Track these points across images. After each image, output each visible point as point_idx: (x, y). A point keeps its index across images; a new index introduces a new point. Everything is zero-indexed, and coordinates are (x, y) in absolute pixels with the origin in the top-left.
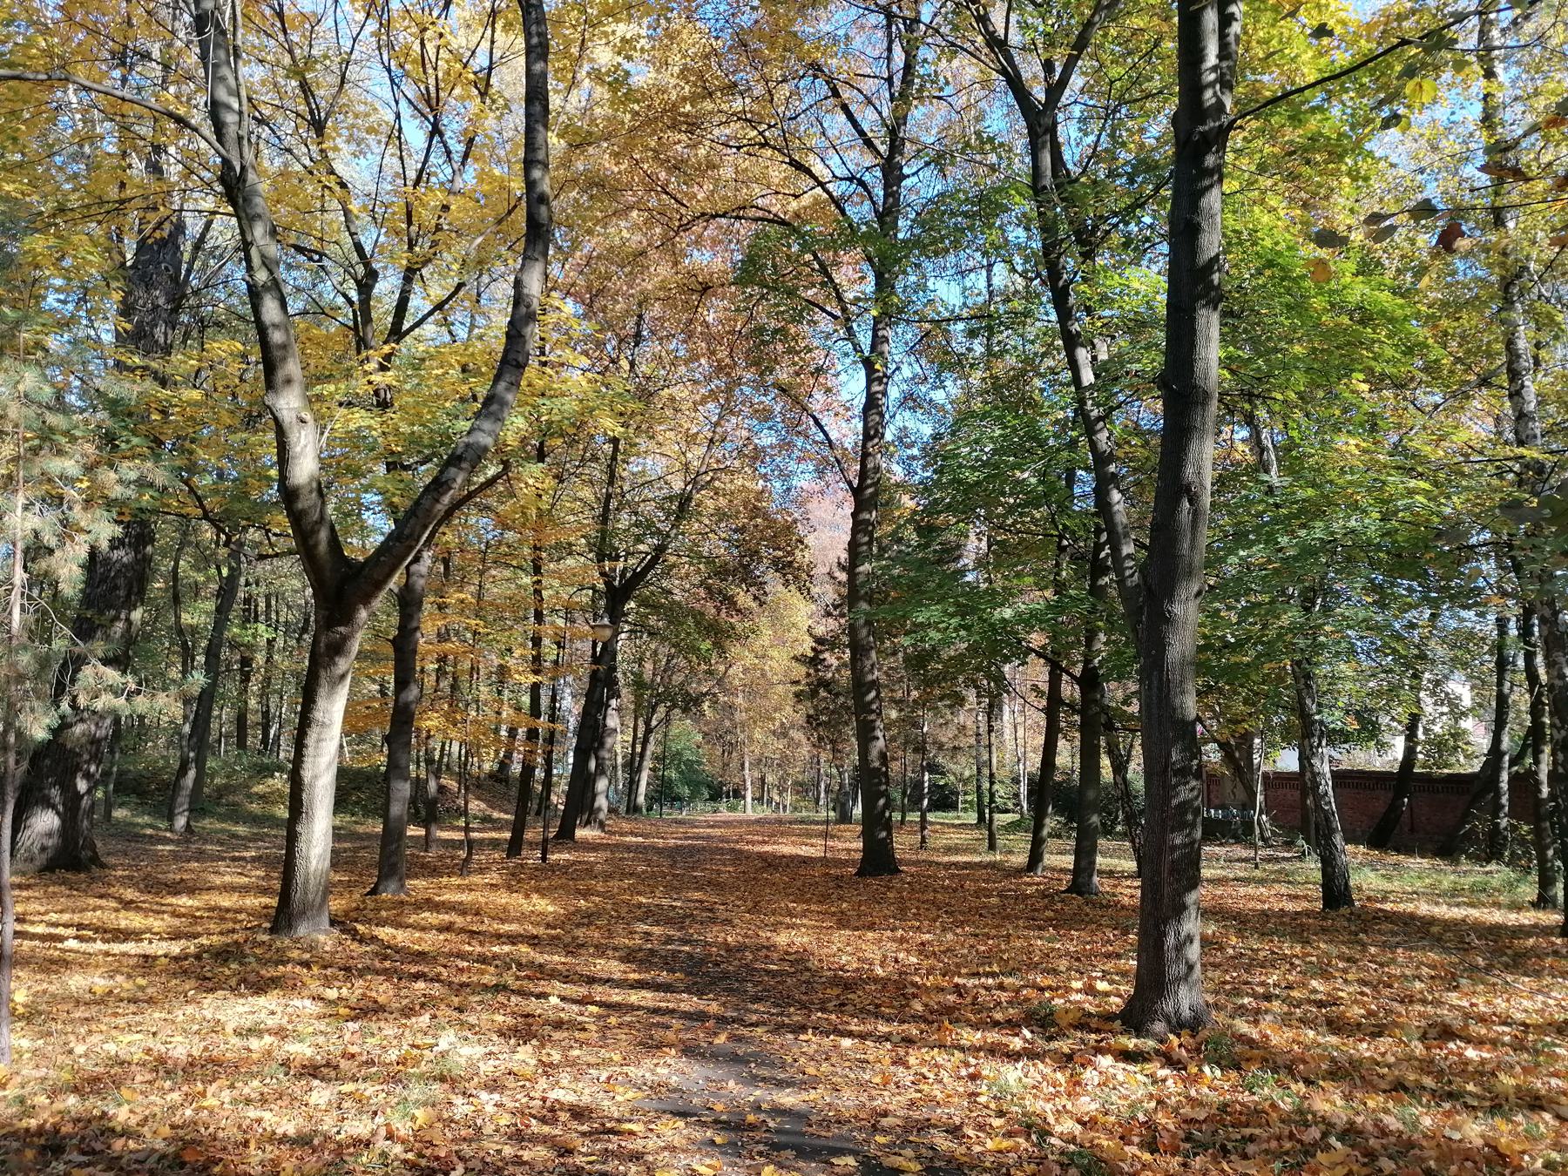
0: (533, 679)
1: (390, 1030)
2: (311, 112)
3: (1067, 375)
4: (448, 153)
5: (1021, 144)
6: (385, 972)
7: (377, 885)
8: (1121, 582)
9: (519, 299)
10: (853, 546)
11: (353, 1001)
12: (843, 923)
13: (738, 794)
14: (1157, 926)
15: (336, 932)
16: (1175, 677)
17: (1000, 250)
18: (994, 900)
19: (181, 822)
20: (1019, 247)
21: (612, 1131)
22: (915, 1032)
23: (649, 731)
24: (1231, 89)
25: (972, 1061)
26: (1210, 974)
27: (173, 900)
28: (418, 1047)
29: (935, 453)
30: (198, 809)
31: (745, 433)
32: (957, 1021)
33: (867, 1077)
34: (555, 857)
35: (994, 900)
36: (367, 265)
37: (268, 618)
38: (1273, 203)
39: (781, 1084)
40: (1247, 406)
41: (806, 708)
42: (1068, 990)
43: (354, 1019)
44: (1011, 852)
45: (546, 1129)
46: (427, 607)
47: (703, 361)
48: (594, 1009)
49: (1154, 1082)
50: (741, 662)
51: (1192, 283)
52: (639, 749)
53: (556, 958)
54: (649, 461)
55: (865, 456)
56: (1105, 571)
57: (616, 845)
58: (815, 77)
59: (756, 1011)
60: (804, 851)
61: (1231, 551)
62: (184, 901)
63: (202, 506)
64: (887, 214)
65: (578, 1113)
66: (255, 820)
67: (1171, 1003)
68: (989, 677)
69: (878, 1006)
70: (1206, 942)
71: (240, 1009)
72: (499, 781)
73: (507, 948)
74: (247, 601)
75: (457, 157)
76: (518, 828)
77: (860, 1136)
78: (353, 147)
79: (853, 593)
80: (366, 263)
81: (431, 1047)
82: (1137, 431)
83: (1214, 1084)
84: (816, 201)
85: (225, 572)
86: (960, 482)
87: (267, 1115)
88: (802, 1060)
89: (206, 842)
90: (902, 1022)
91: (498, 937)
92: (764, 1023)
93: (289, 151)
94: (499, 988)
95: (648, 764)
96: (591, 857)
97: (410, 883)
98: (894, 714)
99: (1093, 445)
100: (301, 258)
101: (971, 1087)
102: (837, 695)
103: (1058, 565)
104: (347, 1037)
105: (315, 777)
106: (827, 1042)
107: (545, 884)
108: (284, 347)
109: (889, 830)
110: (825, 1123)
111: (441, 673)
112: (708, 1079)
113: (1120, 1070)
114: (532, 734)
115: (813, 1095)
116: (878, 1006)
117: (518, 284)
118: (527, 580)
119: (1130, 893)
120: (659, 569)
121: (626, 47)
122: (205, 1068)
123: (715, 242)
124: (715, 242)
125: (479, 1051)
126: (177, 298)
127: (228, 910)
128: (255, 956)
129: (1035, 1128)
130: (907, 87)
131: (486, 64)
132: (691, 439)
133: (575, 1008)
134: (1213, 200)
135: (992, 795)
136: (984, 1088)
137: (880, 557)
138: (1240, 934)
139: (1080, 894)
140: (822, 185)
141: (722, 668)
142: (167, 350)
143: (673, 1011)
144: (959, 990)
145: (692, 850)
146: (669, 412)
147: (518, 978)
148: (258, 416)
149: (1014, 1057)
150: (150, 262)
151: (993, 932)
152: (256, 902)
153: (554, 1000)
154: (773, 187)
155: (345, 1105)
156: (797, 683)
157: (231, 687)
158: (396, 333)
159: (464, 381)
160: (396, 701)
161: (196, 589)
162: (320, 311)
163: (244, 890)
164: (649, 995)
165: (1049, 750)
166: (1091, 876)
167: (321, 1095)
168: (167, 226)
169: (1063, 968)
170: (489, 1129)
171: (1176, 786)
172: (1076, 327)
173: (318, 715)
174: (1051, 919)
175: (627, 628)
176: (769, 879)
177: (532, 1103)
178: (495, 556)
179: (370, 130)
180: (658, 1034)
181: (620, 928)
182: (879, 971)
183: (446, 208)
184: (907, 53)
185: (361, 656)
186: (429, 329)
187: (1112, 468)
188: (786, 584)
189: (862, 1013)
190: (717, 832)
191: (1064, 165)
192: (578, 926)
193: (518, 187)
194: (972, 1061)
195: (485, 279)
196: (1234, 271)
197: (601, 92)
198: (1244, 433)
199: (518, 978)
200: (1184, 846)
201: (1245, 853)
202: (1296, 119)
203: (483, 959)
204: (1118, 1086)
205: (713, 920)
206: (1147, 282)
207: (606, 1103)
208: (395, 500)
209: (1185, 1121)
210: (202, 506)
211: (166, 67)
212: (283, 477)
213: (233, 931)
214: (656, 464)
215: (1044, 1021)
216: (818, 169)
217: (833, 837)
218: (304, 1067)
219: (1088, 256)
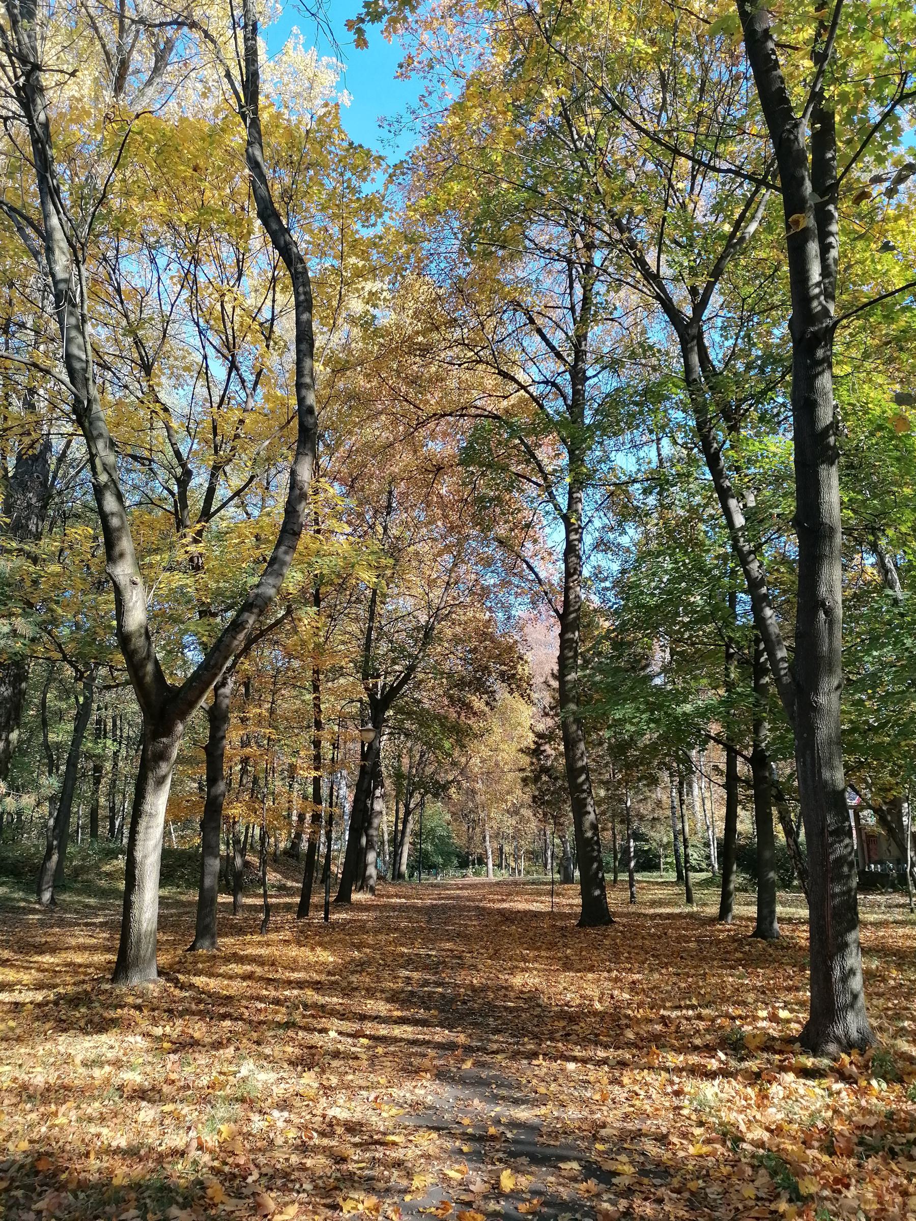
0: (314, 774)
1: (203, 1060)
2: (142, 359)
3: (723, 521)
4: (243, 382)
5: (676, 350)
6: (200, 1013)
7: (195, 942)
8: (778, 680)
9: (294, 484)
10: (562, 660)
11: (175, 1036)
12: (567, 966)
13: (481, 861)
14: (825, 962)
15: (162, 981)
16: (824, 753)
17: (663, 429)
18: (692, 945)
19: (46, 896)
20: (679, 425)
21: (377, 1142)
22: (628, 1056)
23: (408, 813)
24: (833, 298)
25: (677, 1080)
26: (875, 1002)
27: (37, 958)
28: (224, 1074)
29: (624, 588)
30: (59, 886)
31: (473, 576)
32: (664, 1046)
33: (588, 1095)
34: (335, 916)
35: (692, 945)
36: (183, 465)
37: (114, 735)
38: (880, 381)
39: (517, 1102)
40: (871, 538)
41: (532, 790)
42: (755, 1018)
43: (175, 1052)
44: (705, 905)
45: (325, 1142)
46: (234, 718)
47: (439, 523)
48: (364, 1041)
49: (831, 1095)
50: (477, 757)
51: (815, 447)
52: (400, 827)
53: (335, 1000)
54: (401, 601)
55: (567, 589)
56: (765, 672)
57: (385, 906)
58: (515, 310)
59: (496, 1041)
60: (535, 907)
61: (868, 652)
62: (47, 959)
63: (62, 651)
64: (576, 404)
65: (352, 1128)
66: (103, 893)
67: (841, 1027)
68: (679, 760)
69: (597, 1035)
70: (869, 975)
71: (87, 1045)
72: (292, 856)
73: (296, 992)
74: (98, 722)
75: (249, 385)
76: (306, 894)
77: (583, 1145)
78: (173, 381)
79: (564, 697)
80: (183, 465)
81: (234, 1074)
82: (784, 560)
83: (881, 1095)
84: (521, 400)
85: (81, 700)
86: (643, 606)
87: (105, 1131)
88: (534, 1081)
89: (66, 912)
90: (617, 1048)
91: (289, 983)
92: (503, 1051)
93: (126, 387)
94: (289, 1025)
95: (408, 839)
96: (364, 916)
97: (221, 941)
98: (602, 793)
99: (747, 573)
100: (137, 466)
101: (676, 1102)
102: (556, 779)
103: (727, 669)
104: (169, 1066)
105: (145, 857)
106: (555, 1065)
107: (327, 939)
108: (119, 529)
109: (603, 889)
110: (554, 1134)
111: (244, 771)
112: (457, 1098)
113: (802, 1086)
114: (316, 818)
115: (543, 1110)
116: (597, 1035)
117: (293, 473)
118: (309, 697)
119: (803, 936)
120: (411, 684)
121: (372, 298)
122: (58, 1093)
123: (445, 434)
124: (445, 434)
125: (272, 1076)
126: (46, 497)
127: (80, 966)
128: (99, 1001)
129: (730, 1136)
130: (586, 312)
131: (269, 317)
132: (431, 583)
133: (350, 1040)
134: (825, 381)
135: (687, 856)
136: (687, 1102)
137: (584, 668)
138: (899, 967)
139: (764, 938)
140: (524, 388)
141: (463, 760)
142: (38, 536)
143: (429, 1042)
144: (664, 1020)
145: (445, 909)
146: (414, 563)
147: (304, 1016)
148: (105, 583)
149: (711, 1075)
150: (25, 472)
151: (693, 971)
152: (102, 958)
153: (333, 1034)
154: (486, 392)
155: (166, 1122)
156: (522, 770)
157: (85, 788)
158: (206, 514)
159: (258, 548)
160: (209, 793)
161: (60, 714)
162: (149, 502)
163: (92, 949)
164: (409, 1029)
165: (731, 818)
166: (772, 923)
167: (147, 1113)
168: (37, 445)
169: (750, 1000)
170: (279, 1141)
171: (832, 845)
172: (727, 483)
173: (147, 808)
174: (740, 960)
175: (388, 731)
176: (509, 931)
177: (314, 1119)
178: (281, 679)
179: (187, 369)
180: (416, 1061)
181: (386, 974)
182: (598, 1006)
183: (242, 422)
184: (584, 287)
185: (181, 760)
186: (231, 511)
187: (764, 590)
188: (511, 692)
189: (584, 1041)
190: (465, 893)
191: (710, 362)
192: (353, 973)
193: (293, 402)
194: (677, 1080)
195: (273, 471)
196: (851, 435)
197: (356, 332)
198: (871, 560)
199: (304, 1016)
200: (843, 893)
201: (902, 900)
202: (889, 318)
203: (277, 1002)
204: (801, 1100)
205: (462, 966)
206: (780, 446)
207: (374, 1119)
208: (204, 639)
209: (858, 1128)
210: (62, 651)
211: (37, 333)
212: (120, 626)
213: (84, 982)
214: (406, 603)
215: (736, 1046)
216: (521, 377)
217: (558, 895)
218: (135, 1091)
219: (734, 428)
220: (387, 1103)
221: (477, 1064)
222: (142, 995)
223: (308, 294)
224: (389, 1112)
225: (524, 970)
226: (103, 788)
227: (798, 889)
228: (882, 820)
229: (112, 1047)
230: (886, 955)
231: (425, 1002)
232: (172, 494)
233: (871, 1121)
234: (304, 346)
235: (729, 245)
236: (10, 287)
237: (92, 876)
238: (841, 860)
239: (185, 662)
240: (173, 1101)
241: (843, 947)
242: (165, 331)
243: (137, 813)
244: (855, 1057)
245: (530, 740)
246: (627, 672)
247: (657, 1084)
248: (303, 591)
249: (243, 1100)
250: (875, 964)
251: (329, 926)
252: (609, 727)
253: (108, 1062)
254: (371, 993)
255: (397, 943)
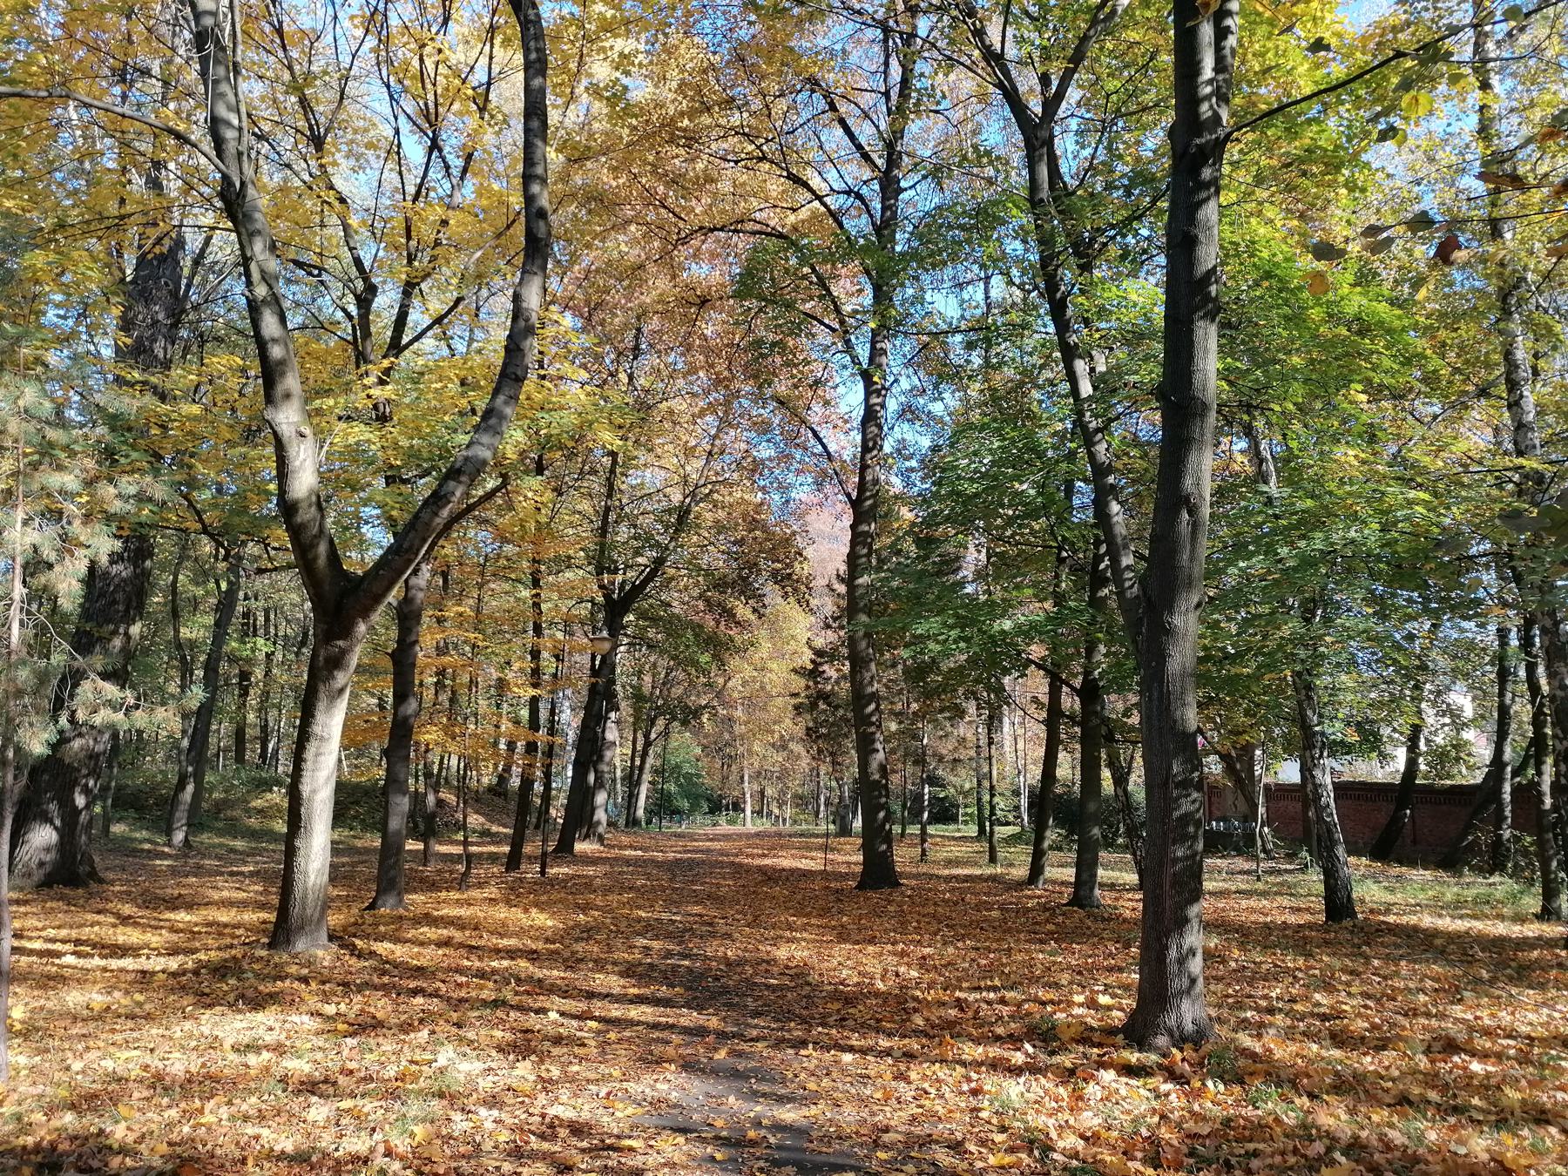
0: (532, 692)
1: (388, 1046)
2: (311, 128)
3: (1065, 387)
4: (447, 167)
5: (1017, 157)
6: (383, 987)
7: (375, 900)
8: (1121, 593)
9: (518, 313)
10: (852, 559)
12: (843, 937)
13: (737, 807)
14: (1159, 939)
15: (334, 947)
17: (999, 263)
19: (179, 836)
21: (611, 1148)
22: (916, 1046)
23: (648, 744)
24: (1227, 101)
25: (974, 1076)
26: (1212, 987)
27: (171, 916)
28: (416, 1063)
29: (933, 465)
31: (743, 446)
32: (959, 1035)
33: (868, 1092)
34: (554, 871)
36: (366, 279)
37: (267, 632)
38: (1270, 215)
39: (781, 1100)
40: (1246, 417)
41: (806, 720)
42: (1070, 1004)
43: (352, 1035)
44: (1011, 865)
45: (546, 1146)
47: (701, 374)
48: (593, 1024)
49: (1157, 1097)
50: (740, 675)
51: (1189, 294)
52: (638, 763)
53: (555, 973)
54: (648, 473)
55: (864, 468)
56: (1104, 582)
58: (813, 91)
59: (756, 1026)
60: (804, 864)
62: (182, 916)
63: (201, 520)
64: (885, 227)
65: (577, 1129)
66: (253, 834)
67: (1173, 1017)
68: (989, 689)
69: (878, 1021)
70: (1208, 955)
71: (239, 1025)
72: (500, 795)
73: (505, 963)
74: (246, 615)
75: (455, 172)
76: (517, 842)
78: (352, 162)
79: (852, 605)
80: (366, 279)
82: (1136, 442)
85: (224, 586)
86: (959, 494)
87: (265, 1132)
88: (803, 1075)
89: (204, 856)
91: (497, 952)
92: (764, 1038)
93: (288, 166)
94: (497, 1004)
95: (647, 777)
96: (590, 871)
97: (410, 897)
98: (893, 727)
99: (1092, 456)
101: (973, 1102)
102: (837, 707)
103: (1057, 576)
104: (346, 1053)
105: (314, 791)
106: (827, 1056)
107: (544, 898)
108: (282, 362)
110: (826, 1139)
111: (439, 686)
112: (708, 1095)
113: (1123, 1085)
114: (531, 748)
115: (814, 1110)
116: (878, 1021)
117: (517, 298)
118: (526, 593)
119: (1131, 906)
121: (623, 62)
122: (203, 1085)
123: (713, 255)
124: (713, 255)
125: (478, 1066)
126: (177, 310)
127: (226, 926)
128: (253, 971)
131: (485, 79)
132: (689, 452)
133: (575, 1023)
134: (1209, 212)
135: (993, 808)
136: (986, 1103)
137: (879, 569)
138: (1242, 946)
139: (1081, 907)
140: (819, 198)
141: (721, 681)
142: (167, 365)
143: (673, 1026)
144: (960, 1004)
147: (516, 993)
148: (257, 430)
149: (1016, 1071)
150: (149, 277)
152: (255, 917)
153: (553, 1015)
154: (770, 201)
155: (343, 1122)
157: (229, 701)
158: (396, 347)
159: (463, 395)
160: (395, 715)
161: (195, 603)
162: (320, 326)
163: (242, 905)
166: (1092, 889)
167: (319, 1111)
169: (1064, 982)
170: (488, 1145)
171: (1179, 798)
172: (1074, 339)
173: (316, 729)
175: (626, 641)
176: (767, 892)
177: (531, 1120)
178: (491, 569)
179: (370, 145)
180: (657, 1049)
181: (619, 943)
182: (880, 985)
183: (445, 223)
185: (360, 669)
186: (428, 343)
187: (1111, 479)
188: (785, 596)
189: (862, 1027)
190: (717, 845)
192: (577, 940)
193: (516, 201)
194: (974, 1076)
197: (599, 107)
199: (516, 993)
200: (1186, 858)
201: (1247, 866)
202: (1292, 132)
203: (481, 974)
205: (713, 935)
206: (1143, 294)
207: (605, 1119)
208: (394, 513)
209: (1188, 1136)
210: (201, 520)
211: (166, 83)
212: (282, 491)
213: (231, 946)
214: (655, 476)
215: (1046, 1036)
216: (816, 182)
217: (832, 850)
218: (302, 1083)
219: (1086, 268)
220: (622, 1101)
221: (733, 1053)
222: (309, 964)
223: (541, 51)
224: (625, 1111)
225: (789, 941)
226: (253, 701)
227: (1124, 849)
228: (1230, 769)
229: (271, 1029)
230: (1226, 932)
231: (669, 976)
232: (350, 317)
233: (1205, 1129)
234: (535, 124)
235: (1094, 22)
236: (128, 17)
237: (237, 813)
238: (1186, 819)
239: (362, 542)
240: (353, 1096)
241: (1182, 923)
242: (342, 93)
243: (304, 736)
244: (1189, 1053)
245: (806, 658)
246: (932, 574)
247: (950, 1080)
248: (522, 454)
249: (441, 1095)
250: (1214, 942)
251: (547, 883)
252: (906, 646)
253: (267, 1047)
254: (600, 965)
255: (632, 905)
